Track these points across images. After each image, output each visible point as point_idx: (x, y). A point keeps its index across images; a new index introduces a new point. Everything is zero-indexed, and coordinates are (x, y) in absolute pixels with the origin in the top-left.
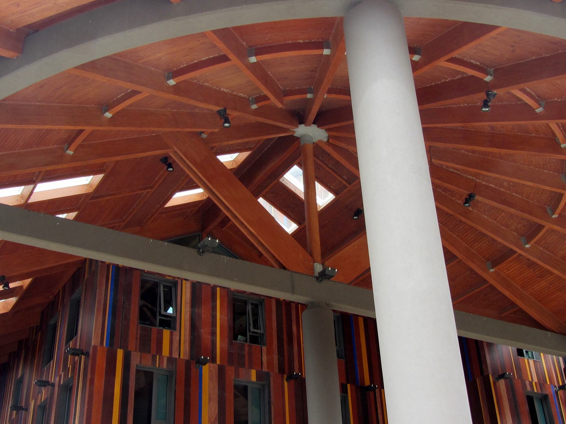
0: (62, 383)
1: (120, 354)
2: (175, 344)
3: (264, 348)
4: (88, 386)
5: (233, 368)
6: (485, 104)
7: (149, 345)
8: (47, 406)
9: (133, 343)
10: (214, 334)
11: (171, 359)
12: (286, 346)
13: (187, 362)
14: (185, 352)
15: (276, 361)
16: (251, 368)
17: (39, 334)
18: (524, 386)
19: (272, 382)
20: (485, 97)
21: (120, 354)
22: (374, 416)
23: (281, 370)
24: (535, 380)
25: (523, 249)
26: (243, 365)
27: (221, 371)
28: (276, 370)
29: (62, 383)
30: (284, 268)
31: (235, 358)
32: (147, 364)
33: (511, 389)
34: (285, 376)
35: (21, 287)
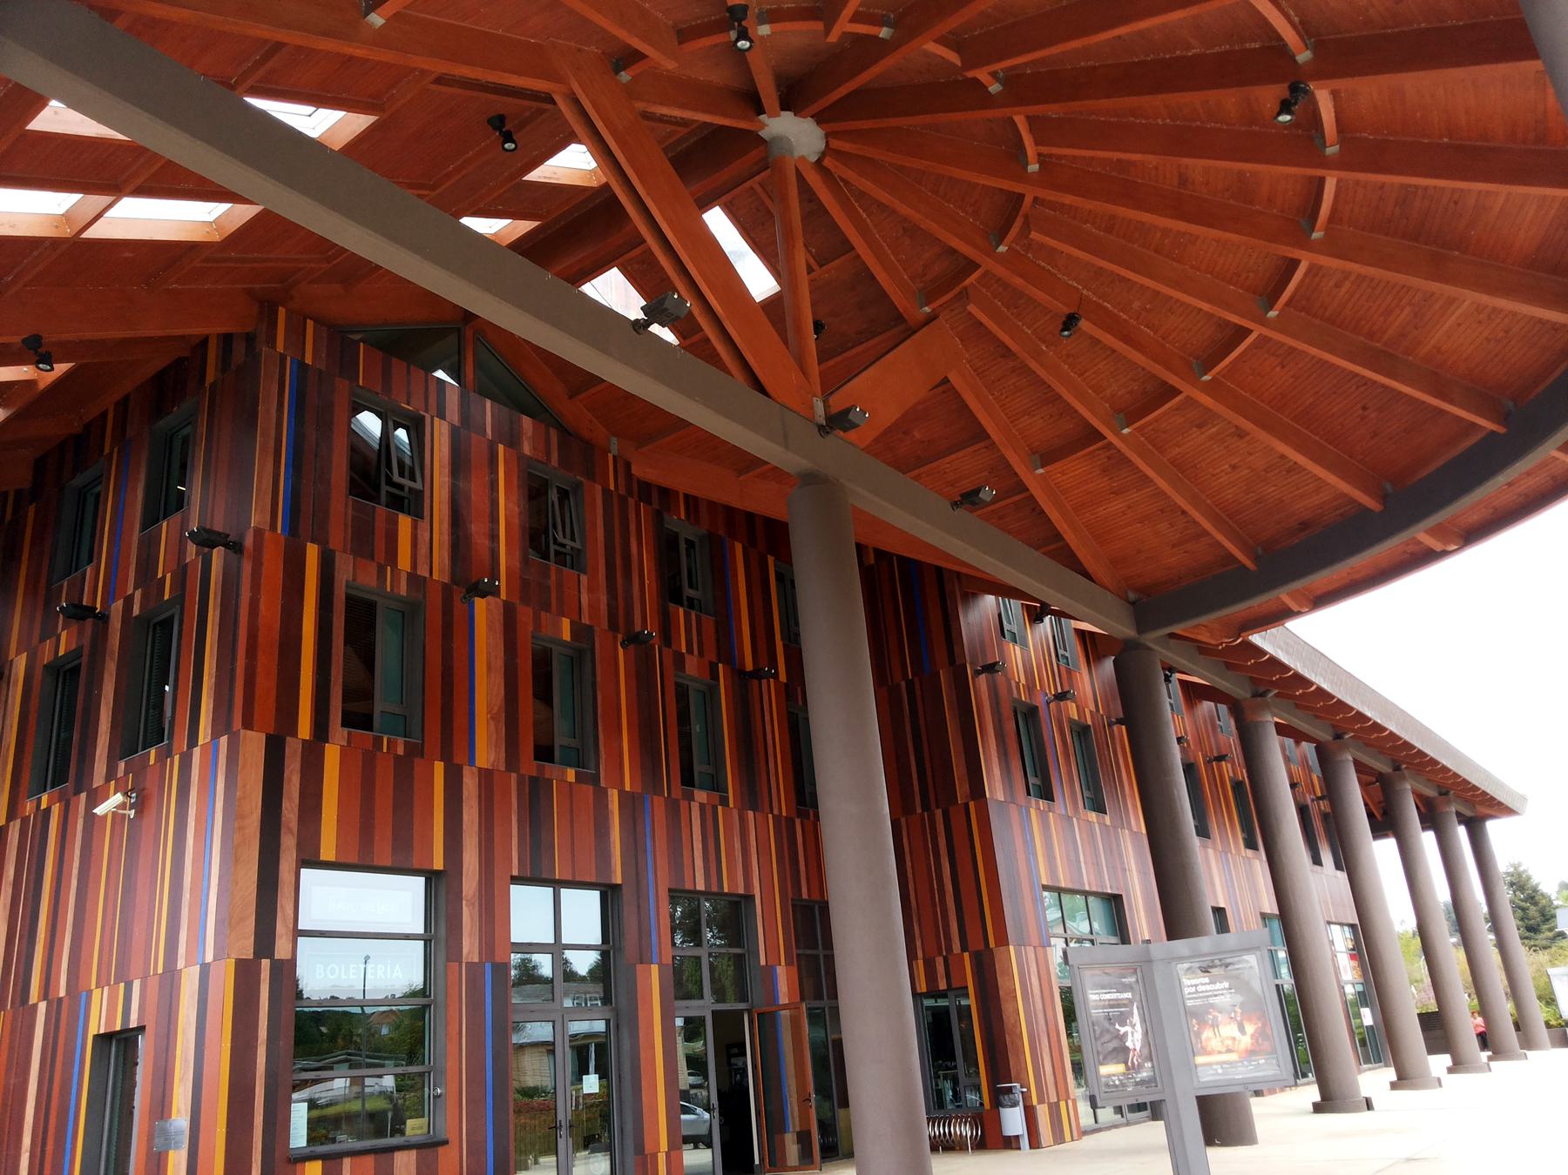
0: (136, 611)
1: (312, 552)
2: (420, 547)
3: (584, 579)
5: (530, 611)
6: (1285, 107)
7: (370, 543)
8: (84, 660)
10: (494, 537)
11: (413, 578)
12: (620, 580)
14: (440, 567)
15: (603, 607)
17: (32, 509)
20: (1287, 94)
21: (312, 552)
22: (759, 725)
23: (613, 626)
24: (1023, 681)
25: (1118, 434)
27: (509, 612)
28: (605, 625)
29: (136, 611)
30: (763, 391)
31: (532, 591)
32: (368, 579)
33: (994, 690)
34: (620, 637)
35: (29, 384)
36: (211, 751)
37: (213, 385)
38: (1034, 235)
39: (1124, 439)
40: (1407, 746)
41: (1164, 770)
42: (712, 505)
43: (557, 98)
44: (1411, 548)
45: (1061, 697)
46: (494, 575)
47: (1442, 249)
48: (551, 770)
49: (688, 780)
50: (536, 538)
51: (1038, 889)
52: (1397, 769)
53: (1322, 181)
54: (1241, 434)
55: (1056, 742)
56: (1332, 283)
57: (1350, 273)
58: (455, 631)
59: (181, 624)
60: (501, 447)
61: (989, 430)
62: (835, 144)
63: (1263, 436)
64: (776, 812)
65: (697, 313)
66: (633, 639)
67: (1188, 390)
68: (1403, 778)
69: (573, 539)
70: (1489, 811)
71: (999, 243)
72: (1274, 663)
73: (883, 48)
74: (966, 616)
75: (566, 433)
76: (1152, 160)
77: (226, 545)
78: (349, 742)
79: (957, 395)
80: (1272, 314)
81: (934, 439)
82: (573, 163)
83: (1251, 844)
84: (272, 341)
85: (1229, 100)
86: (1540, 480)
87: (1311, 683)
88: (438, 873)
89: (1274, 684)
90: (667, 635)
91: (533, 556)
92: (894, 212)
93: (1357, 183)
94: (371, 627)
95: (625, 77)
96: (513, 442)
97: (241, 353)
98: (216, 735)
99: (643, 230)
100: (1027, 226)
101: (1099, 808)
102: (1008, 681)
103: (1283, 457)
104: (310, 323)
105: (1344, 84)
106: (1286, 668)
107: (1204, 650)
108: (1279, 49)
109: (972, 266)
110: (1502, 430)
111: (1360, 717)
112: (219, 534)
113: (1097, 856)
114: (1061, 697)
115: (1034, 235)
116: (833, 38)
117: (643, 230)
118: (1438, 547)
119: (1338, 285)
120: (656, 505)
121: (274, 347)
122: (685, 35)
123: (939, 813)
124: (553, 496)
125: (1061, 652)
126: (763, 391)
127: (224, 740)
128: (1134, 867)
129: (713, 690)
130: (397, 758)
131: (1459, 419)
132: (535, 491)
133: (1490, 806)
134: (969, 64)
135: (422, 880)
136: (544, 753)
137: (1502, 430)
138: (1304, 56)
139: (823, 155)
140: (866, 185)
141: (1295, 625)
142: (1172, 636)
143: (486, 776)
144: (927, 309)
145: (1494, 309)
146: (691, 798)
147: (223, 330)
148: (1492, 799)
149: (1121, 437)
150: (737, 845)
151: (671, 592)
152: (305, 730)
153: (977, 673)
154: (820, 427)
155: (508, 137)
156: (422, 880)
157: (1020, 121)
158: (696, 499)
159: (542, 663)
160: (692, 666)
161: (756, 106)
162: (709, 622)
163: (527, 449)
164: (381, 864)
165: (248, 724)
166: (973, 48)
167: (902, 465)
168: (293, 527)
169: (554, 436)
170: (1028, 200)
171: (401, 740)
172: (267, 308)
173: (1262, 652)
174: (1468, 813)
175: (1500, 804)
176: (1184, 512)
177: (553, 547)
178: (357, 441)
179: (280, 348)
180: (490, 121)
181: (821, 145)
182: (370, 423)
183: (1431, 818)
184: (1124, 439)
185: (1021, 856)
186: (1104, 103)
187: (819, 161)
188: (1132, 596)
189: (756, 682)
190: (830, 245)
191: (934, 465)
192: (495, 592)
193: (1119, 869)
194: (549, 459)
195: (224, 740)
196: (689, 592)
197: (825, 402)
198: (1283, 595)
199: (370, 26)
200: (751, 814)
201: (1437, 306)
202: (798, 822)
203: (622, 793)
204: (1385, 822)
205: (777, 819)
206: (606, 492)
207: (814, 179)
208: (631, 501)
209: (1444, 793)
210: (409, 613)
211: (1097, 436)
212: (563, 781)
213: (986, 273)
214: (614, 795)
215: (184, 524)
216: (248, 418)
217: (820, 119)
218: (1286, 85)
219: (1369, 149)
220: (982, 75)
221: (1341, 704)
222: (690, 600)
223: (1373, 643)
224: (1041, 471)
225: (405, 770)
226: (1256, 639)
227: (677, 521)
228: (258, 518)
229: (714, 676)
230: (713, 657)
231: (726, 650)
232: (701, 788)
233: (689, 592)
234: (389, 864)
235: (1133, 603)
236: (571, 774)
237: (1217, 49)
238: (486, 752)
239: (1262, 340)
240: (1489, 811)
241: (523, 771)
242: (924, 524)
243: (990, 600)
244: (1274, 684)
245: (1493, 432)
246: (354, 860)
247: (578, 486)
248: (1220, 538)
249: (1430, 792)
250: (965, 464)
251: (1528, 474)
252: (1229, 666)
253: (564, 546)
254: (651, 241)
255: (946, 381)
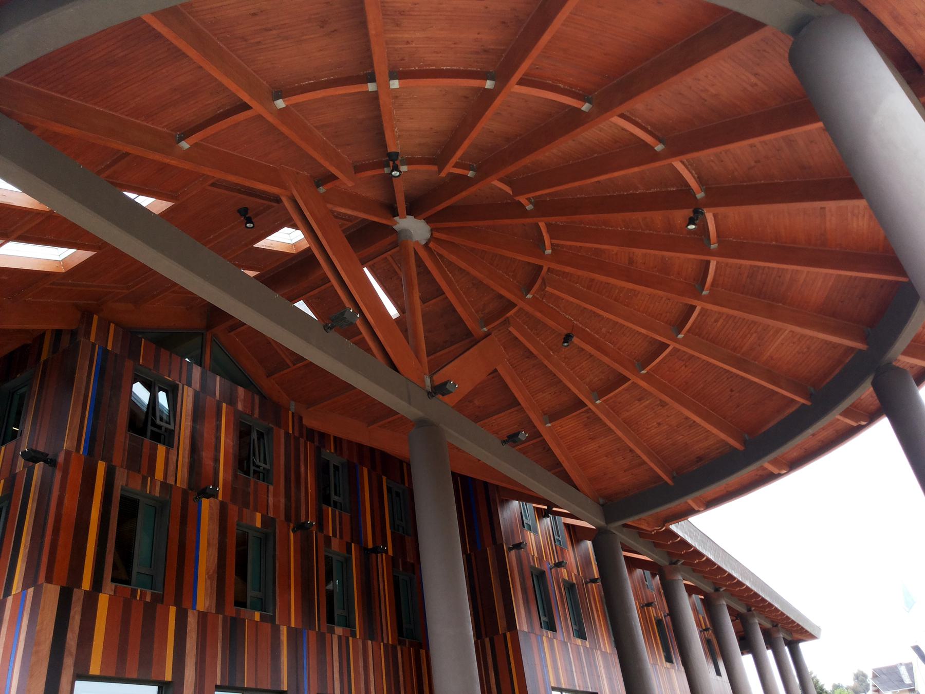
1: (101, 467)
2: (170, 465)
3: (271, 488)
4: (293, 505)
6: (692, 221)
7: (139, 462)
9: (118, 457)
10: (217, 460)
11: (165, 485)
12: (293, 489)
13: (184, 492)
14: (181, 479)
15: (282, 506)
16: (256, 510)
18: (529, 562)
19: (277, 531)
21: (101, 467)
23: (288, 519)
24: (536, 555)
25: (593, 403)
26: (246, 505)
27: (223, 507)
28: (283, 517)
30: (396, 369)
31: (239, 495)
32: (135, 485)
34: (292, 525)
36: (22, 597)
37: (46, 362)
38: (548, 289)
39: (597, 406)
40: (756, 595)
41: (626, 610)
42: (350, 442)
43: (284, 199)
44: (760, 472)
45: (559, 565)
46: (216, 484)
47: (772, 301)
48: (245, 612)
49: (331, 620)
50: (243, 462)
51: (549, 689)
52: (749, 610)
53: (708, 263)
54: (663, 404)
55: (556, 593)
56: (713, 320)
57: (723, 314)
58: (188, 519)
59: (7, 512)
60: (224, 405)
61: (520, 401)
62: (437, 235)
63: (677, 406)
64: (385, 641)
65: (359, 323)
66: (301, 527)
67: (634, 378)
68: (753, 616)
69: (265, 463)
70: (799, 637)
71: (528, 293)
72: (684, 543)
73: (469, 182)
74: (502, 511)
75: (263, 397)
76: (615, 249)
77: (46, 461)
78: (115, 592)
79: (502, 380)
80: (680, 336)
81: (491, 402)
82: (287, 238)
83: (669, 659)
84: (88, 334)
85: (657, 217)
86: (829, 433)
87: (703, 555)
88: (168, 683)
89: (682, 556)
90: (321, 525)
91: (240, 473)
92: (468, 273)
93: (727, 264)
94: (135, 516)
95: (322, 190)
96: (232, 402)
97: (65, 344)
98: (25, 587)
99: (330, 274)
100: (544, 284)
101: (582, 635)
102: (528, 555)
103: (687, 418)
104: (112, 326)
105: (721, 210)
106: (690, 546)
107: (642, 534)
108: (687, 191)
109: (512, 305)
110: (808, 403)
111: (730, 577)
112: (42, 453)
113: (582, 667)
114: (559, 565)
115: (548, 289)
116: (443, 175)
117: (330, 274)
118: (776, 471)
119: (716, 321)
120: (317, 444)
121: (89, 338)
122: (358, 169)
123: (487, 640)
124: (254, 436)
125: (556, 537)
126: (396, 369)
127: (31, 591)
128: (604, 675)
129: (348, 560)
130: (146, 603)
131: (784, 397)
132: (243, 433)
133: (801, 633)
134: (517, 192)
135: (156, 688)
136: (240, 603)
137: (808, 403)
138: (700, 195)
139: (429, 241)
140: (453, 258)
141: (694, 520)
142: (625, 526)
143: (203, 617)
144: (485, 329)
145: (802, 335)
146: (332, 632)
147: (56, 327)
148: (803, 628)
149: (596, 405)
150: (361, 664)
151: (324, 498)
152: (86, 584)
153: (510, 549)
154: (429, 393)
155: (249, 220)
156: (156, 688)
157: (542, 225)
158: (341, 439)
159: (242, 543)
160: (335, 544)
161: (393, 211)
162: (347, 517)
163: (240, 407)
164: (130, 677)
165: (49, 580)
166: (519, 184)
167: (477, 419)
168: (90, 451)
169: (257, 399)
170: (545, 269)
171: (149, 593)
172: (87, 315)
173: (677, 536)
174: (789, 638)
175: (807, 632)
176: (631, 451)
177: (252, 468)
178: (133, 404)
179: (92, 339)
180: (239, 211)
181: (428, 235)
182: (141, 392)
183: (771, 643)
184: (597, 406)
185: (538, 668)
186: (591, 217)
187: (426, 245)
188: (601, 501)
189: (374, 555)
190: (432, 292)
191: (486, 421)
192: (214, 495)
193: (595, 676)
194: (253, 413)
195: (31, 591)
196: (336, 498)
197: (431, 378)
198: (690, 500)
199: (180, 148)
200: (370, 642)
201: (771, 332)
202: (399, 648)
203: (289, 629)
204: (747, 645)
205: (385, 646)
206: (287, 434)
207: (423, 254)
208: (302, 441)
209: (775, 626)
210: (160, 507)
211: (583, 405)
212: (252, 620)
213: (521, 309)
214: (284, 630)
215: (17, 448)
216: (68, 381)
217: (428, 220)
218: (691, 210)
219: (734, 246)
220: (522, 199)
221: (720, 569)
222: (335, 503)
223: (736, 531)
224: (549, 425)
225: (151, 613)
226: (673, 527)
227: (329, 453)
228: (68, 444)
229: (349, 551)
230: (347, 538)
231: (357, 534)
232: (339, 625)
233: (334, 498)
234: (135, 676)
235: (602, 505)
236: (257, 616)
237: (652, 190)
238: (204, 600)
239: (676, 350)
240: (799, 637)
241: (227, 614)
242: (486, 453)
243: (515, 504)
244: (682, 556)
245: (803, 404)
246: (112, 674)
247: (269, 430)
248: (652, 465)
249: (768, 625)
250: (506, 420)
251: (823, 429)
252: (656, 545)
253: (259, 467)
254: (334, 282)
255: (496, 370)
